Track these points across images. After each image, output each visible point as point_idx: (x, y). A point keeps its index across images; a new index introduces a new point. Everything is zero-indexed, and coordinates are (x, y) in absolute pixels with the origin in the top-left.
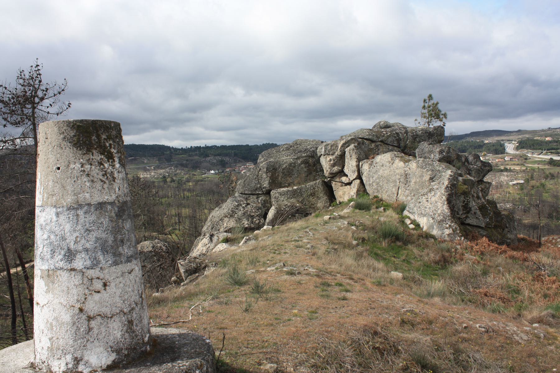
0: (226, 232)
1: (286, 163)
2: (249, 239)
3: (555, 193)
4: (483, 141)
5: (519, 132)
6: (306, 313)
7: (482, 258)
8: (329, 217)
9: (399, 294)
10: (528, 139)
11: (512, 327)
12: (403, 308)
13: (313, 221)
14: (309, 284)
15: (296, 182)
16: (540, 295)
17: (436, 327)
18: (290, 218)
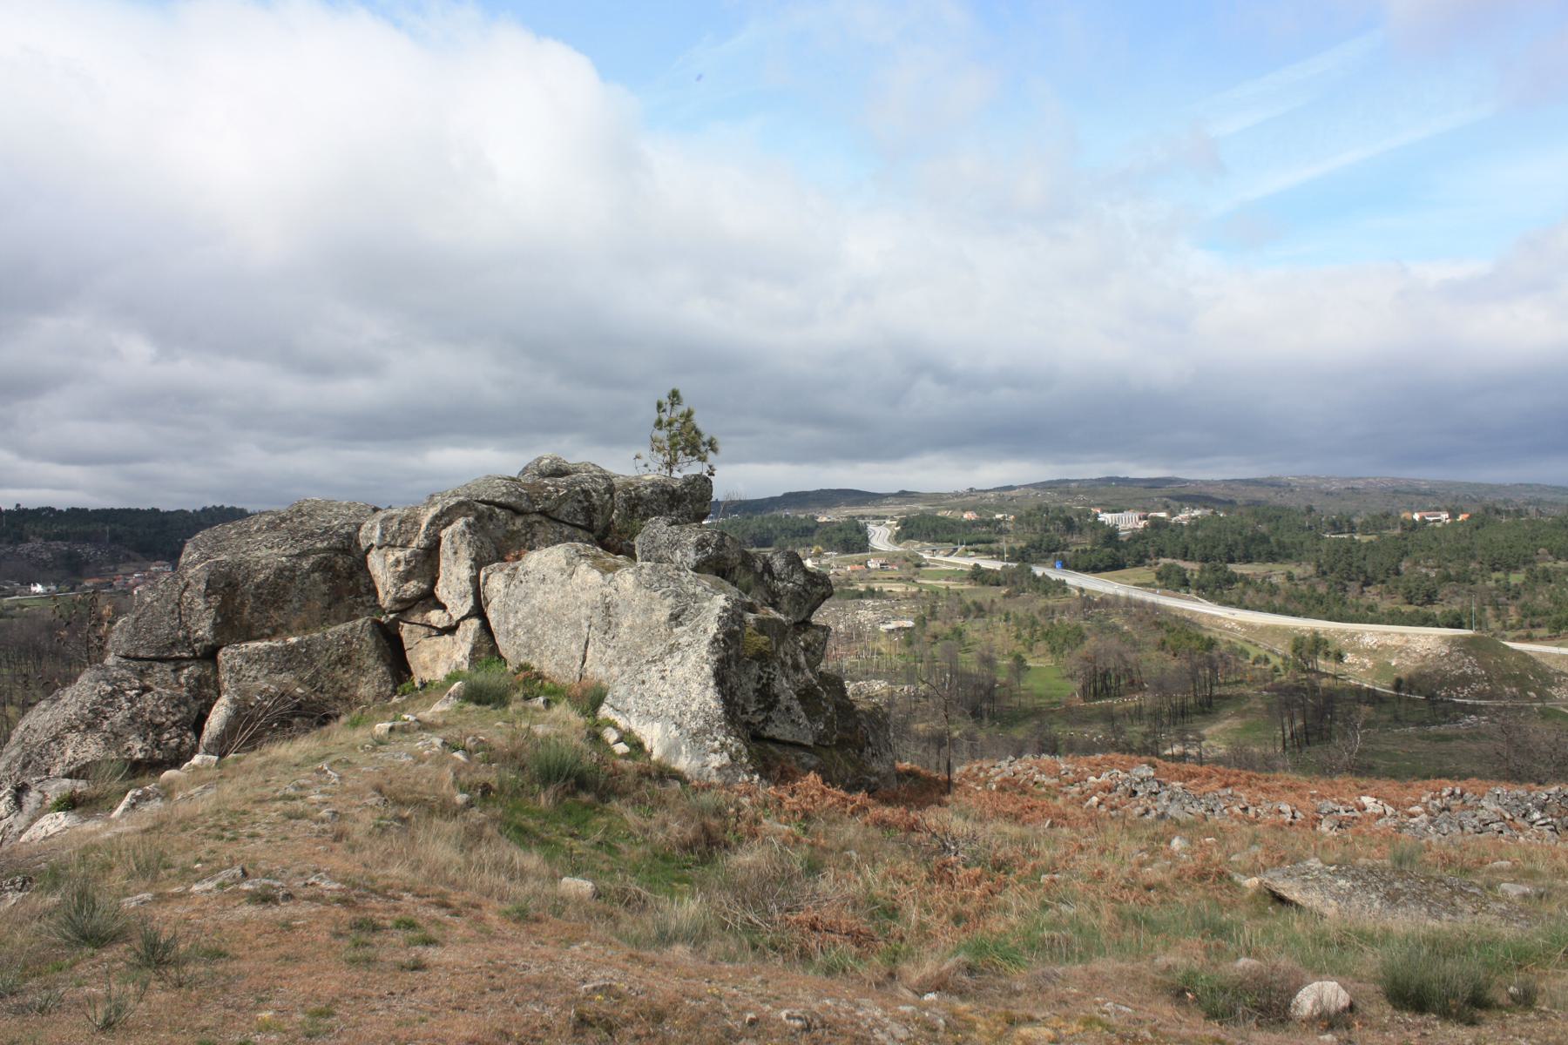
0: (69, 776)
1: (266, 566)
2: (145, 798)
4: (813, 518)
5: (904, 495)
6: (299, 1017)
7: (805, 829)
8: (389, 725)
9: (578, 941)
10: (923, 516)
11: (871, 1010)
12: (584, 981)
13: (341, 739)
14: (316, 927)
15: (294, 624)
16: (945, 917)
17: (674, 1027)
18: (274, 730)
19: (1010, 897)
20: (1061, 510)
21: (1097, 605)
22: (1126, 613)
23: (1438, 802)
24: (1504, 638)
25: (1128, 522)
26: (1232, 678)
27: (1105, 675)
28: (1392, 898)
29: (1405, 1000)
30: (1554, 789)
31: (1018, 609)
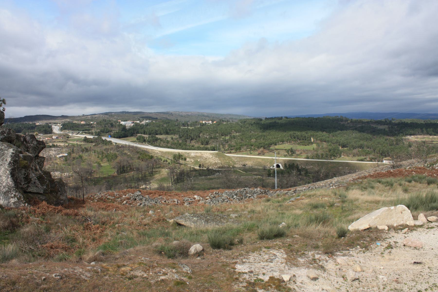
3: (89, 162)
4: (35, 124)
5: (63, 117)
7: (44, 219)
10: (69, 122)
11: (79, 270)
16: (90, 240)
17: (19, 286)
19: (108, 232)
20: (110, 121)
21: (120, 147)
22: (129, 149)
23: (212, 195)
24: (225, 153)
25: (129, 124)
26: (158, 166)
27: (123, 167)
28: (207, 221)
29: (215, 246)
30: (238, 190)
31: (98, 149)
